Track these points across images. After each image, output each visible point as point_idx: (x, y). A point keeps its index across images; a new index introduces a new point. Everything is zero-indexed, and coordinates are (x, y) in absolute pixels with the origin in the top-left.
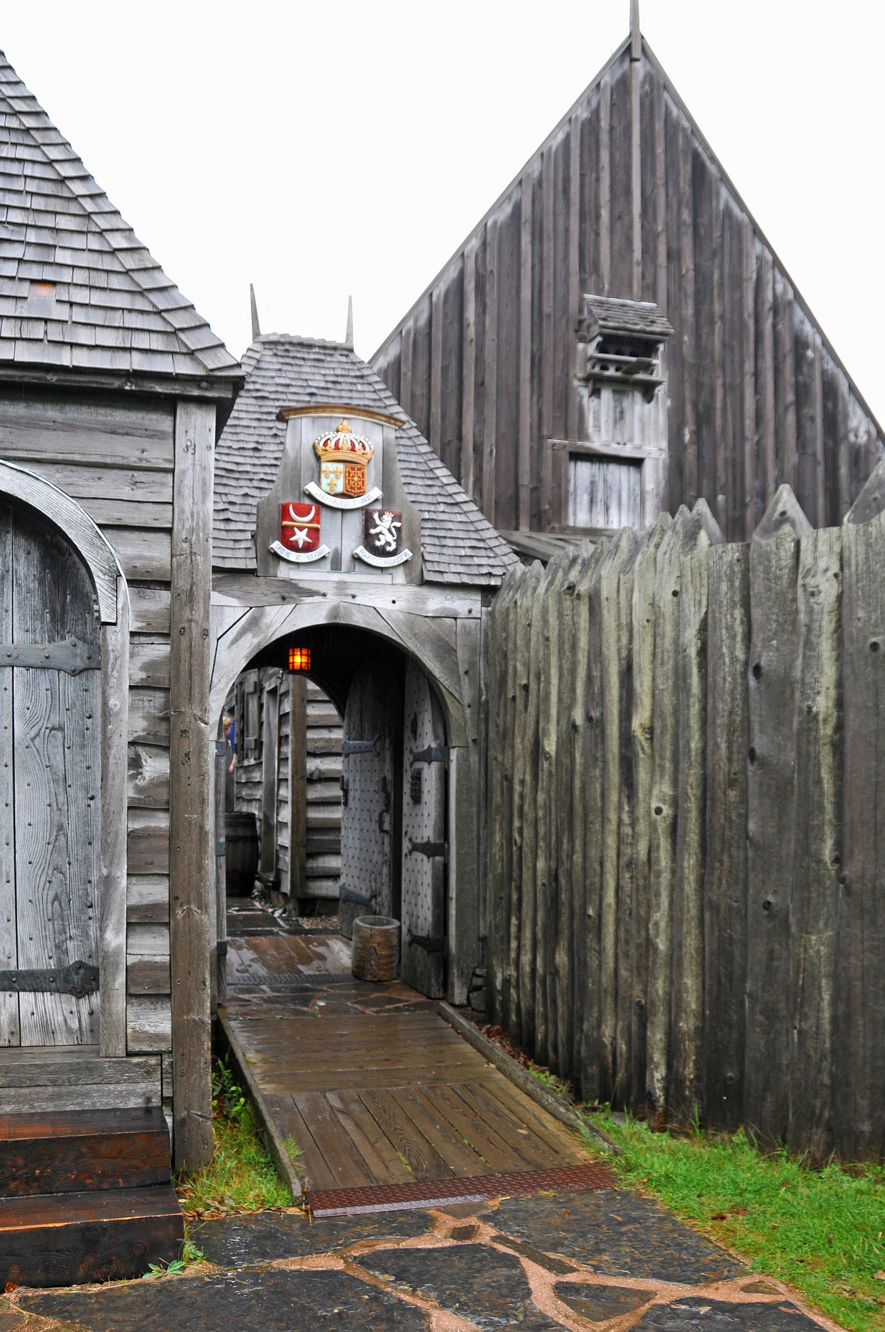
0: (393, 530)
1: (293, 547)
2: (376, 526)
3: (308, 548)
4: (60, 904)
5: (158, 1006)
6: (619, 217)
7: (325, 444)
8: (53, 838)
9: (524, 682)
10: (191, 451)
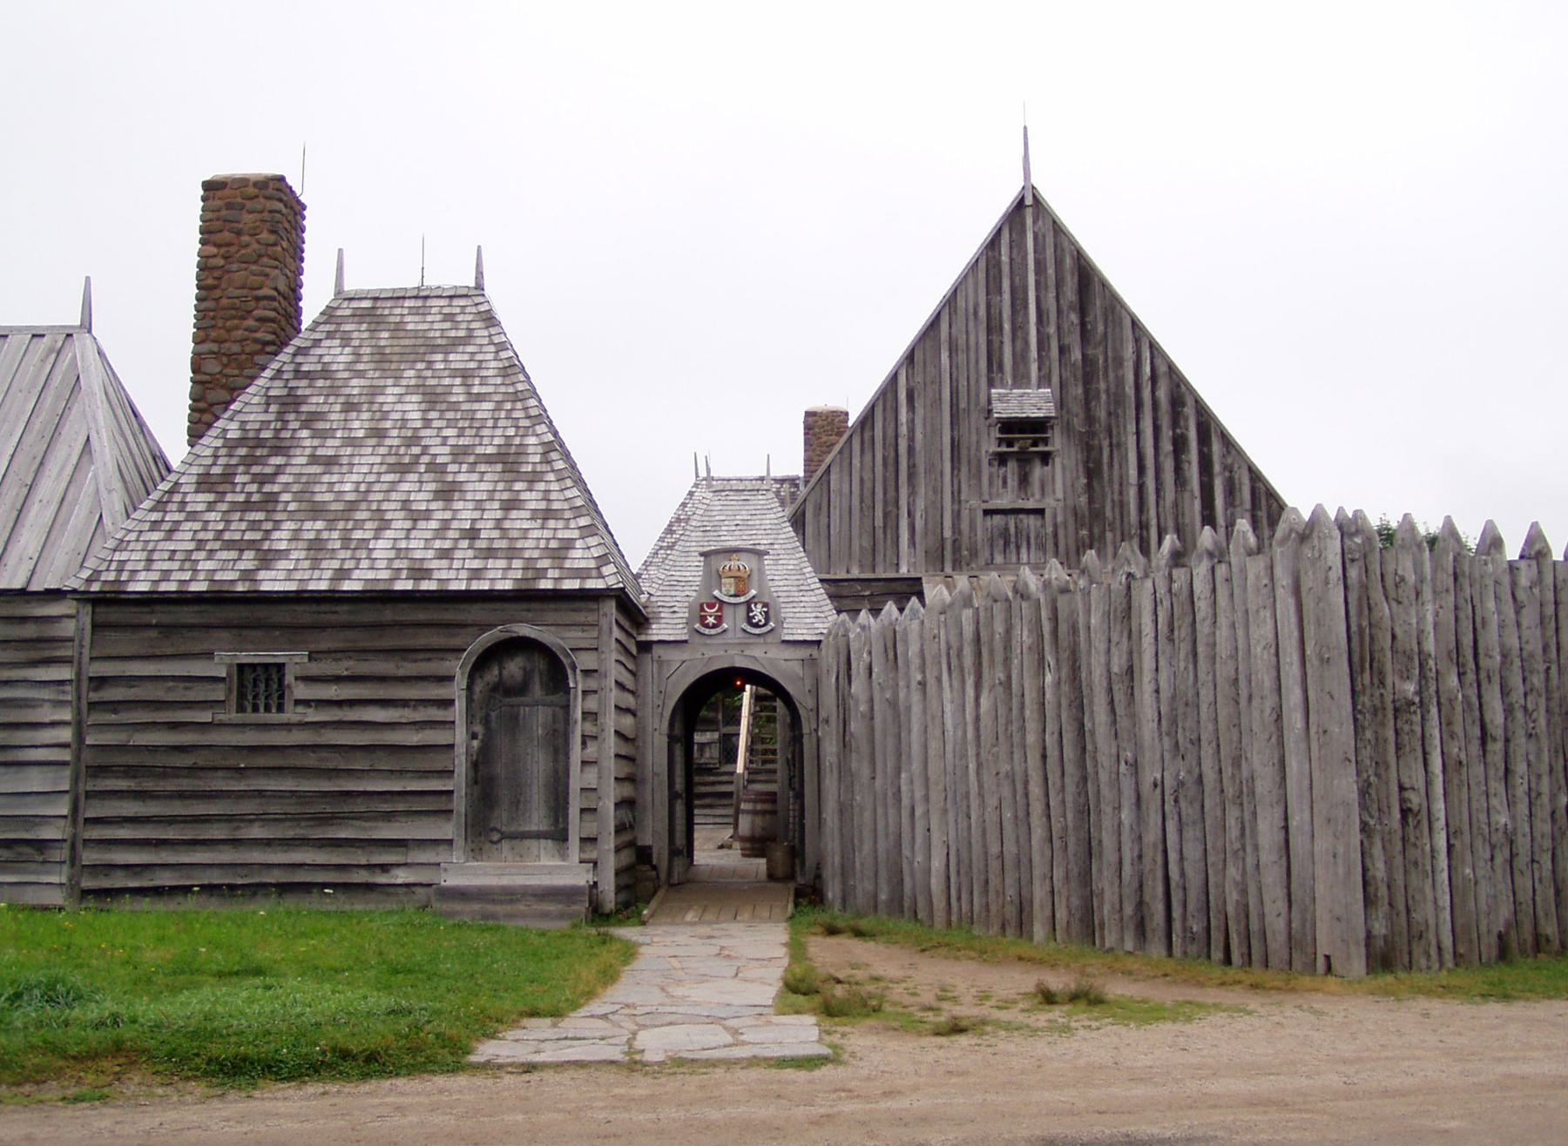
1: (707, 626)
3: (714, 626)
6: (1018, 329)
9: (919, 677)
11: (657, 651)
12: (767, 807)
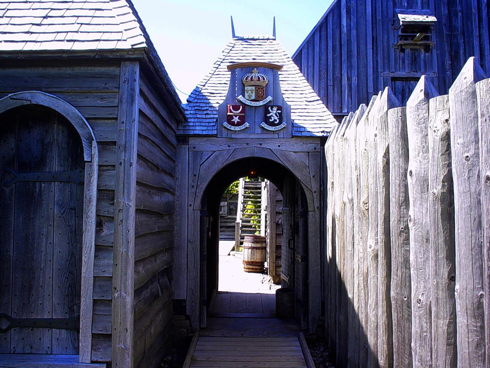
0: (278, 114)
1: (233, 124)
2: (270, 113)
3: (239, 124)
4: (71, 289)
5: (107, 339)
7: (246, 79)
8: (69, 258)
10: (127, 82)
11: (192, 141)
12: (258, 245)
